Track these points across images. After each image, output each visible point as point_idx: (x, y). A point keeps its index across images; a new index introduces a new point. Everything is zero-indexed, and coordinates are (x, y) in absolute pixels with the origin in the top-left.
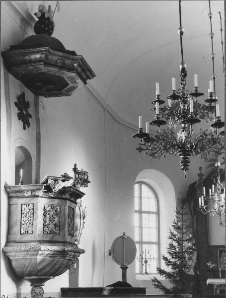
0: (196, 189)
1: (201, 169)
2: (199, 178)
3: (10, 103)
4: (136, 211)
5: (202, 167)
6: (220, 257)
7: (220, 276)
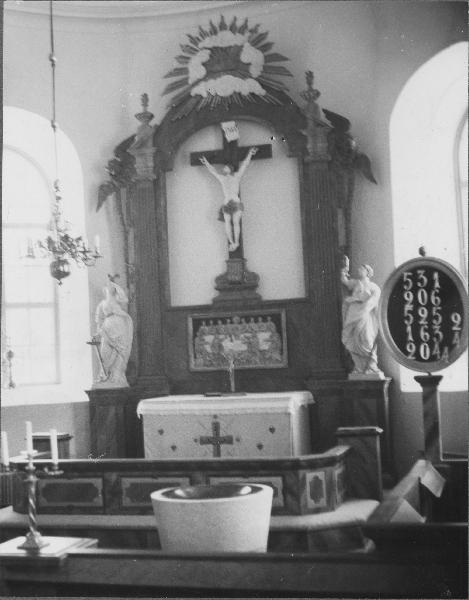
0: (133, 157)
1: (145, 99)
2: (139, 123)
3: (221, 190)
4: (218, 453)
5: (148, 93)
6: (195, 336)
7: (233, 384)
